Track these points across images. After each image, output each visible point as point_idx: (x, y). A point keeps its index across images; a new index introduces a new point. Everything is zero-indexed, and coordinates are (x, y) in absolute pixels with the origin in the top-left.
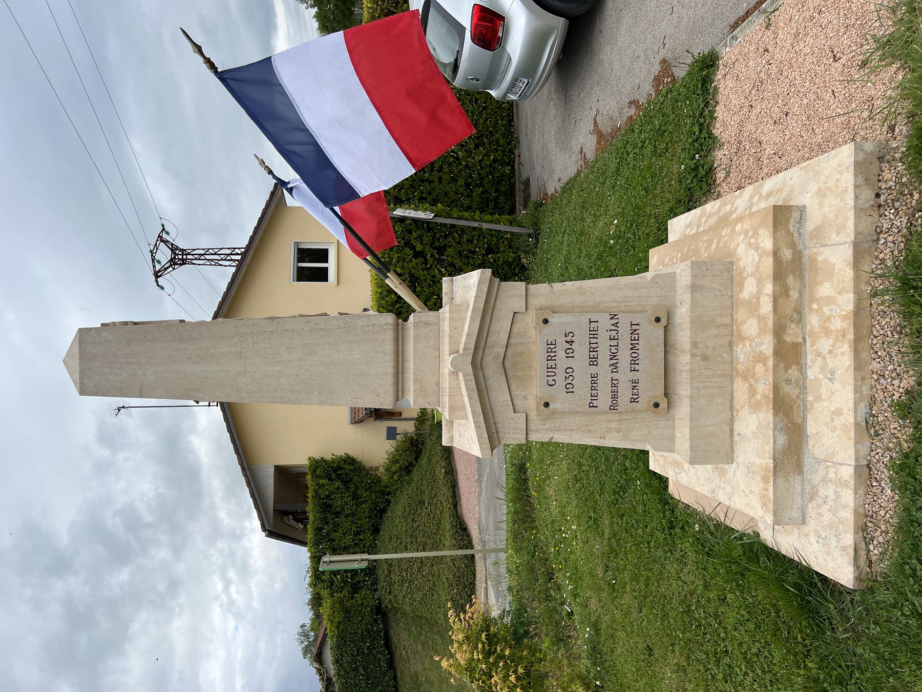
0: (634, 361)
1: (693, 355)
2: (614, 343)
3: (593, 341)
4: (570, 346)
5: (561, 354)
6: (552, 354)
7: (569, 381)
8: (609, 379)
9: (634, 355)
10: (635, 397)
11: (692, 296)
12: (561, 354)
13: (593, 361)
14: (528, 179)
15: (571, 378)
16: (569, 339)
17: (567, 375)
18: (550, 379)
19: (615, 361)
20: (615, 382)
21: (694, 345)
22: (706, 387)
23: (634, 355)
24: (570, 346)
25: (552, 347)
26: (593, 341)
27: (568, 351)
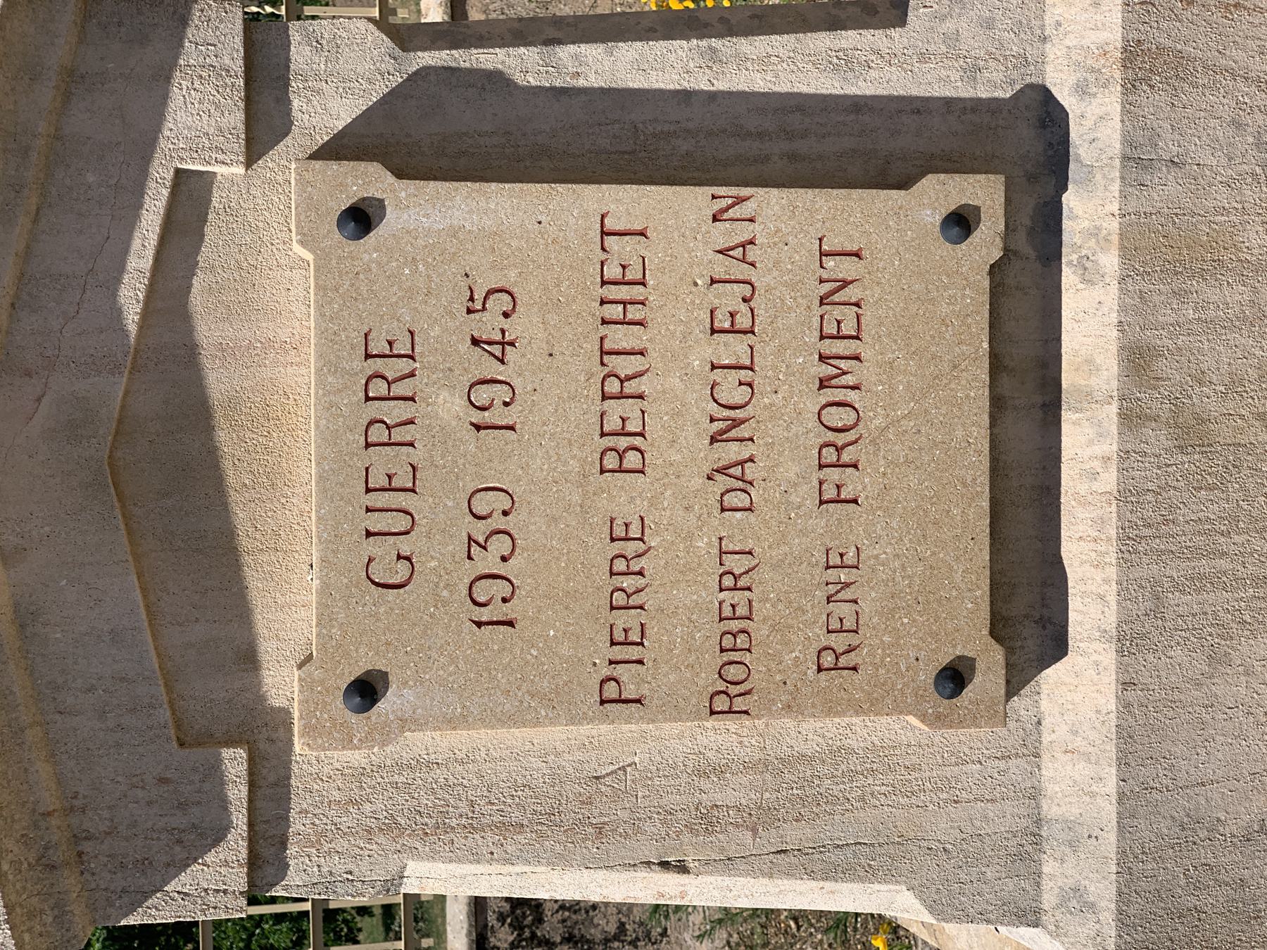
0: (836, 454)
1: (1131, 419)
2: (733, 349)
3: (620, 337)
4: (492, 369)
5: (446, 406)
6: (628, 583)
7: (488, 562)
8: (704, 544)
9: (838, 417)
10: (839, 642)
11: (1129, 110)
12: (446, 406)
13: (621, 452)
14: (508, 899)
15: (500, 545)
16: (489, 325)
17: (480, 530)
18: (383, 549)
19: (733, 452)
20: (737, 564)
21: (1138, 360)
22: (1198, 582)
23: (838, 417)
24: (492, 369)
25: (393, 368)
26: (620, 337)
27: (483, 395)
